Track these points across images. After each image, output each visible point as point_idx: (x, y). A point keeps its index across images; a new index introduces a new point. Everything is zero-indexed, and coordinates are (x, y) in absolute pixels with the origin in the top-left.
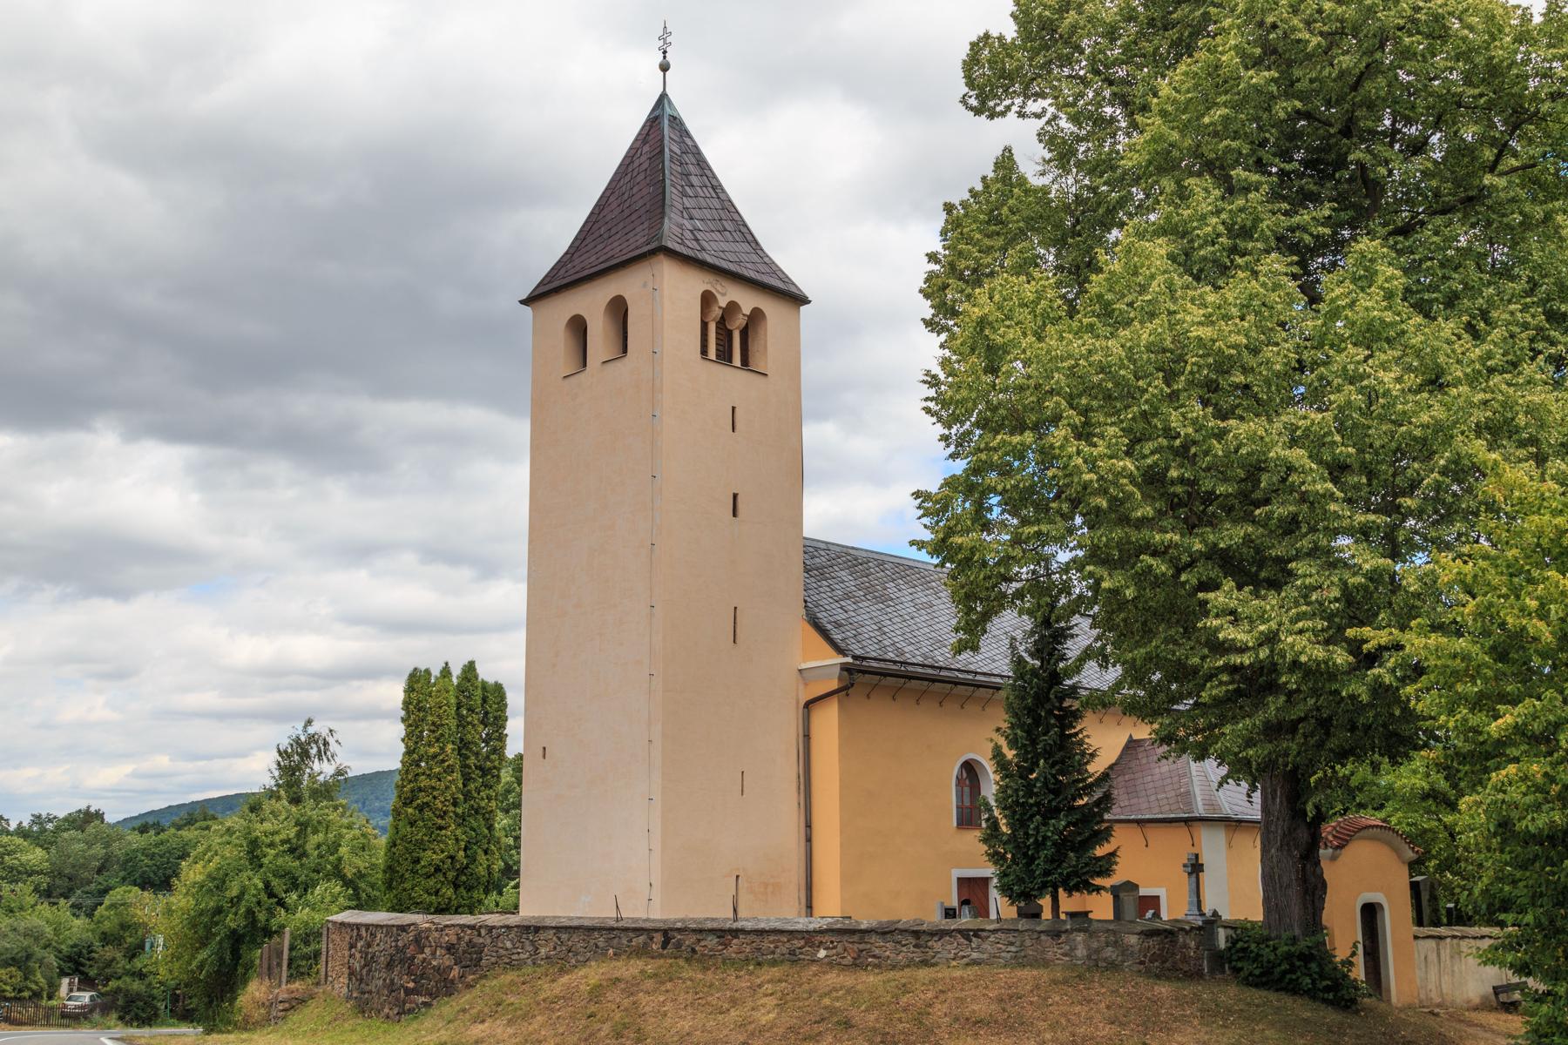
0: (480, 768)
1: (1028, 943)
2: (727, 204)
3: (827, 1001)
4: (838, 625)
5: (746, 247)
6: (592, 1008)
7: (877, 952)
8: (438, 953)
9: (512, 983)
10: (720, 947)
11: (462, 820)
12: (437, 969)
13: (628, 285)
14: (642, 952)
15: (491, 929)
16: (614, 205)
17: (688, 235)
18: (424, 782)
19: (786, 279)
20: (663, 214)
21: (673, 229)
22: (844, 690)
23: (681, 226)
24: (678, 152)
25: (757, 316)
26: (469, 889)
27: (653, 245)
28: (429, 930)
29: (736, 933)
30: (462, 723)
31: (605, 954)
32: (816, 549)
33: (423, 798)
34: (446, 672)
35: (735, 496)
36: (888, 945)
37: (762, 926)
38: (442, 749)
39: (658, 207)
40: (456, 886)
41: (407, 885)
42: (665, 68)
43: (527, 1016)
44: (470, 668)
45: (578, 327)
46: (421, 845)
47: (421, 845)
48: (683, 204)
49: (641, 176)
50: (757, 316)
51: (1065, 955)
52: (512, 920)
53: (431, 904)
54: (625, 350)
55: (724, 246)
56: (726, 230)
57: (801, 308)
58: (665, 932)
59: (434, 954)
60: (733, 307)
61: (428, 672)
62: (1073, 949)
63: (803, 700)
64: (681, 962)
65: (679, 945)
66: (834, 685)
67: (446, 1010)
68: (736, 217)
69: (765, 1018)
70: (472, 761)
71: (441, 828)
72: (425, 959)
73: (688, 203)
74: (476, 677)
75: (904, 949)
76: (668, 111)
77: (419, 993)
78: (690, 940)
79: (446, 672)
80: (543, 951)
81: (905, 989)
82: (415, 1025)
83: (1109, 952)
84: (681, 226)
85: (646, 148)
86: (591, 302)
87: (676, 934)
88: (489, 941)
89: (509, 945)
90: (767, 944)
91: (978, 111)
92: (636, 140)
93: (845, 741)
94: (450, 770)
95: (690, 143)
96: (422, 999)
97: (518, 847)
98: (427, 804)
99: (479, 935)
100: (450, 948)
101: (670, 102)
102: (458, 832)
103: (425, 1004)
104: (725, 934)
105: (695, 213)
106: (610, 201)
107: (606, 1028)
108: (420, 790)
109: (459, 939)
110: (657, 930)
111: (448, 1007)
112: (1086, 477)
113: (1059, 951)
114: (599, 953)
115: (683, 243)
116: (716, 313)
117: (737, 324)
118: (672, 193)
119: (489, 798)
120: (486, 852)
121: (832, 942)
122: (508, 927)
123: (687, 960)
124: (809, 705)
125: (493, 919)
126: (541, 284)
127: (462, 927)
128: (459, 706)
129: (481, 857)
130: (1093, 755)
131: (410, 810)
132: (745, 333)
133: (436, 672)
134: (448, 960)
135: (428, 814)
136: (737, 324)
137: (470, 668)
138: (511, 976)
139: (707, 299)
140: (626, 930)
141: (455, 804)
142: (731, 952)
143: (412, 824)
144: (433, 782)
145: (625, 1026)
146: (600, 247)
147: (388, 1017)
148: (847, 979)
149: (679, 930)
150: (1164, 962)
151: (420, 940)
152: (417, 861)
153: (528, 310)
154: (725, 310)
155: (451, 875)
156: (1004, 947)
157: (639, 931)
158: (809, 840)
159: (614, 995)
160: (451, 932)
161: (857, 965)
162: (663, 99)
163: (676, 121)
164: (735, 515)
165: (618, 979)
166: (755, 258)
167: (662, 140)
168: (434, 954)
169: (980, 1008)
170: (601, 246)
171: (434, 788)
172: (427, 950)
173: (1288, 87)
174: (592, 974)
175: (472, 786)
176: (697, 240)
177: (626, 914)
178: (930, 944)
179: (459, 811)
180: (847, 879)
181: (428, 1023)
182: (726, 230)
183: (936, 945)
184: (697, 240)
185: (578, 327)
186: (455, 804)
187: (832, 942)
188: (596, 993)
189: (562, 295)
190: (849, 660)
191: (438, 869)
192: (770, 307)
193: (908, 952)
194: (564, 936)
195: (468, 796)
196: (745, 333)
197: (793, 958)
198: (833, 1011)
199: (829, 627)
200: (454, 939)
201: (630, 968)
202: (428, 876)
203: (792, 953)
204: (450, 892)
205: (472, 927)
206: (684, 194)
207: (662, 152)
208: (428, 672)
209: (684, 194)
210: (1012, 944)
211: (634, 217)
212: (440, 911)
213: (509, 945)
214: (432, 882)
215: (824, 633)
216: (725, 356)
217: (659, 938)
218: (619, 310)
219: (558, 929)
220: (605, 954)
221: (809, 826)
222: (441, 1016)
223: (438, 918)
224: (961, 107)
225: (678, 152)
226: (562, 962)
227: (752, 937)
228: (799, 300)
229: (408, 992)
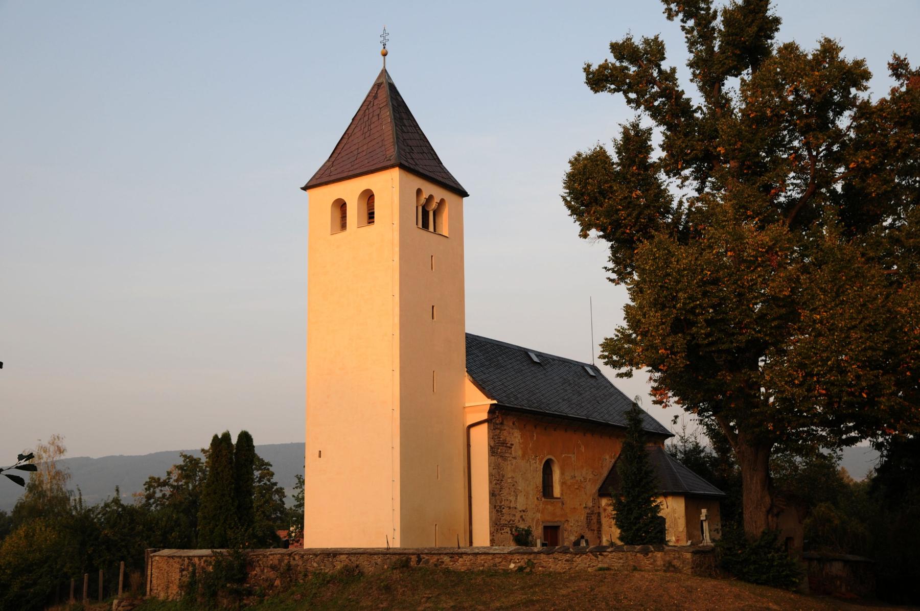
1: (630, 558)
7: (544, 564)
8: (265, 571)
10: (451, 563)
24: (396, 105)
36: (550, 560)
45: (341, 205)
48: (403, 137)
50: (442, 202)
51: (651, 564)
56: (424, 153)
57: (464, 198)
58: (418, 555)
59: (262, 571)
62: (655, 561)
72: (256, 574)
75: (560, 562)
87: (425, 556)
88: (301, 563)
99: (294, 559)
106: (355, 132)
110: (413, 554)
113: (648, 562)
116: (423, 200)
121: (518, 559)
134: (272, 574)
136: (434, 205)
139: (419, 192)
149: (426, 554)
150: (701, 568)
156: (617, 561)
162: (384, 72)
170: (354, 159)
176: (413, 159)
178: (574, 559)
182: (424, 153)
184: (413, 159)
185: (341, 205)
187: (518, 559)
189: (329, 186)
192: (449, 197)
200: (276, 562)
210: (621, 559)
225: (396, 105)
227: (471, 557)
228: (463, 194)
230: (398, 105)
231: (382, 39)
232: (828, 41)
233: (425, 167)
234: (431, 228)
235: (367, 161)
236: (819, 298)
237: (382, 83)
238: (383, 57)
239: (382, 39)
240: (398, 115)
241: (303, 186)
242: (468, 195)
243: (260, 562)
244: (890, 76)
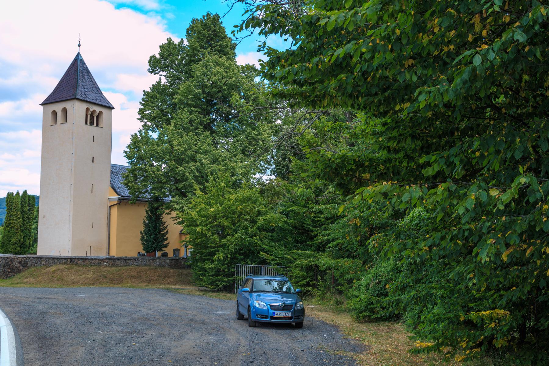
0: (27, 218)
2: (94, 83)
3: (103, 273)
4: (119, 188)
5: (99, 95)
6: (53, 275)
9: (35, 270)
11: (22, 231)
12: (16, 267)
13: (68, 105)
14: (65, 263)
15: (30, 258)
16: (65, 82)
17: (83, 93)
18: (12, 221)
19: (109, 103)
20: (77, 88)
21: (79, 93)
22: (119, 204)
23: (81, 91)
25: (101, 113)
26: (24, 248)
27: (74, 97)
28: (14, 258)
29: (87, 259)
30: (22, 206)
31: (57, 264)
32: (116, 167)
33: (12, 225)
34: (18, 193)
35: (93, 158)
37: (93, 258)
38: (17, 213)
39: (76, 86)
40: (21, 247)
41: (7, 247)
42: (79, 46)
43: (38, 277)
44: (25, 192)
45: (55, 113)
46: (11, 237)
47: (11, 237)
49: (72, 75)
50: (101, 113)
52: (35, 256)
53: (14, 252)
54: (66, 122)
55: (93, 95)
59: (15, 264)
60: (94, 111)
61: (13, 193)
63: (109, 205)
64: (74, 265)
65: (74, 262)
66: (116, 203)
67: (19, 276)
68: (97, 86)
69: (89, 276)
70: (25, 216)
71: (16, 233)
73: (84, 84)
74: (27, 194)
76: (80, 58)
77: (12, 273)
78: (76, 261)
79: (18, 193)
80: (42, 263)
81: (119, 270)
82: (11, 280)
83: (163, 263)
84: (81, 91)
85: (74, 68)
86: (58, 108)
89: (34, 262)
90: (93, 262)
91: (151, 72)
92: (71, 64)
93: (119, 216)
94: (19, 218)
95: (85, 67)
96: (12, 274)
97: (37, 234)
98: (13, 227)
100: (20, 262)
101: (80, 55)
102: (21, 234)
103: (13, 275)
104: (84, 259)
105: (85, 87)
107: (56, 279)
108: (11, 223)
109: (22, 260)
111: (19, 276)
112: (153, 175)
114: (56, 264)
115: (81, 96)
116: (90, 113)
117: (95, 115)
118: (80, 82)
119: (30, 225)
120: (29, 239)
122: (34, 258)
123: (76, 265)
124: (110, 207)
125: (30, 256)
126: (45, 100)
127: (23, 258)
128: (22, 202)
129: (28, 240)
130: (165, 223)
131: (8, 228)
132: (98, 117)
133: (15, 193)
134: (19, 265)
135: (13, 229)
136: (96, 114)
137: (25, 192)
138: (34, 268)
139: (87, 109)
140: (62, 258)
141: (20, 227)
142: (85, 263)
143: (9, 232)
144: (14, 221)
145: (60, 278)
146: (61, 93)
147: (3, 278)
148: (109, 269)
151: (12, 260)
152: (10, 241)
153: (42, 106)
154: (92, 113)
155: (19, 245)
157: (65, 259)
158: (109, 238)
159: (58, 272)
160: (20, 259)
161: (112, 266)
162: (79, 54)
163: (82, 61)
164: (93, 162)
165: (59, 269)
166: (101, 98)
167: (78, 66)
168: (15, 264)
169: (133, 274)
170: (61, 93)
171: (15, 223)
172: (14, 263)
173: (204, 92)
174: (53, 268)
175: (25, 222)
176: (85, 95)
177: (62, 255)
179: (22, 228)
180: (117, 247)
181: (14, 279)
183: (129, 262)
184: (85, 95)
185: (55, 113)
186: (20, 227)
188: (54, 272)
190: (120, 197)
191: (16, 243)
192: (104, 111)
193: (123, 263)
194: (47, 260)
195: (24, 225)
196: (98, 117)
197: (99, 265)
198: (103, 275)
199: (116, 188)
200: (21, 260)
201: (62, 267)
202: (13, 245)
203: (99, 263)
204: (19, 249)
205: (25, 258)
206: (83, 82)
207: (77, 70)
208: (13, 193)
209: (83, 82)
211: (70, 87)
212: (16, 253)
213: (34, 262)
214: (14, 246)
215: (115, 190)
216: (92, 123)
217: (69, 260)
218: (65, 111)
219: (46, 258)
220: (57, 264)
221: (109, 235)
222: (17, 278)
223: (16, 255)
224: (148, 72)
226: (47, 266)
228: (111, 108)
229: (9, 272)
234: (95, 124)
236: (386, 127)
243: (449, 335)
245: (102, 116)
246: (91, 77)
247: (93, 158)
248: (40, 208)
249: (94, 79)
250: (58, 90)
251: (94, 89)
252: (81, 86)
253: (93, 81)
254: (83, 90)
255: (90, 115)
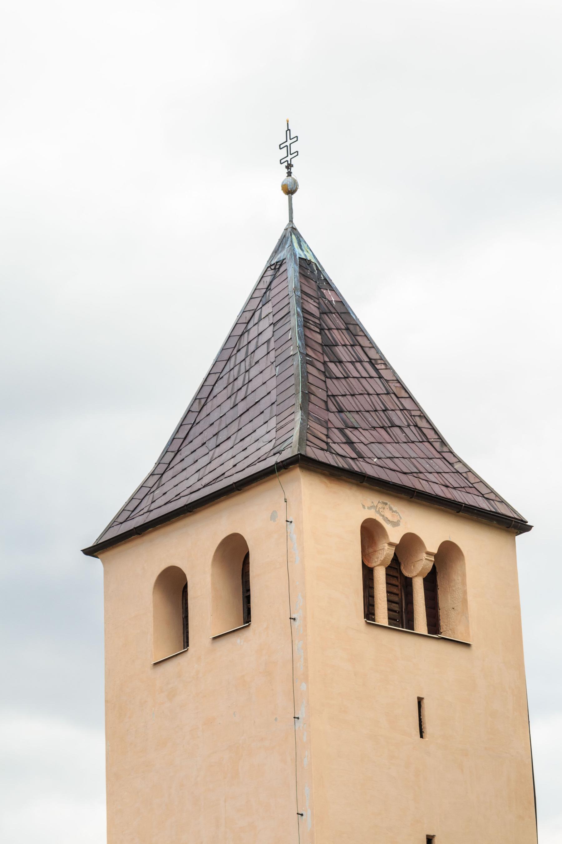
2: (394, 386)
24: (316, 312)
35: (420, 701)
49: (263, 351)
56: (393, 425)
57: (517, 537)
68: (407, 404)
73: (336, 387)
101: (299, 238)
115: (329, 449)
153: (96, 563)
162: (292, 230)
164: (422, 736)
166: (440, 465)
176: (350, 443)
182: (393, 425)
184: (350, 443)
225: (316, 312)
230: (322, 313)
231: (284, 152)
232: (427, 836)
233: (390, 463)
235: (196, 476)
237: (281, 263)
238: (286, 197)
239: (284, 152)
240: (318, 338)
241: (90, 543)
242: (529, 528)
244: (533, 526)
245: (456, 578)
246: (372, 354)
247: (420, 701)
248: (336, 286)
249: (387, 366)
250: (186, 451)
251: (398, 418)
252: (323, 395)
253: (385, 374)
254: (334, 419)
255: (389, 569)
